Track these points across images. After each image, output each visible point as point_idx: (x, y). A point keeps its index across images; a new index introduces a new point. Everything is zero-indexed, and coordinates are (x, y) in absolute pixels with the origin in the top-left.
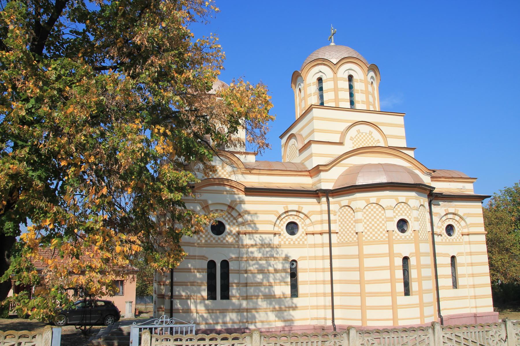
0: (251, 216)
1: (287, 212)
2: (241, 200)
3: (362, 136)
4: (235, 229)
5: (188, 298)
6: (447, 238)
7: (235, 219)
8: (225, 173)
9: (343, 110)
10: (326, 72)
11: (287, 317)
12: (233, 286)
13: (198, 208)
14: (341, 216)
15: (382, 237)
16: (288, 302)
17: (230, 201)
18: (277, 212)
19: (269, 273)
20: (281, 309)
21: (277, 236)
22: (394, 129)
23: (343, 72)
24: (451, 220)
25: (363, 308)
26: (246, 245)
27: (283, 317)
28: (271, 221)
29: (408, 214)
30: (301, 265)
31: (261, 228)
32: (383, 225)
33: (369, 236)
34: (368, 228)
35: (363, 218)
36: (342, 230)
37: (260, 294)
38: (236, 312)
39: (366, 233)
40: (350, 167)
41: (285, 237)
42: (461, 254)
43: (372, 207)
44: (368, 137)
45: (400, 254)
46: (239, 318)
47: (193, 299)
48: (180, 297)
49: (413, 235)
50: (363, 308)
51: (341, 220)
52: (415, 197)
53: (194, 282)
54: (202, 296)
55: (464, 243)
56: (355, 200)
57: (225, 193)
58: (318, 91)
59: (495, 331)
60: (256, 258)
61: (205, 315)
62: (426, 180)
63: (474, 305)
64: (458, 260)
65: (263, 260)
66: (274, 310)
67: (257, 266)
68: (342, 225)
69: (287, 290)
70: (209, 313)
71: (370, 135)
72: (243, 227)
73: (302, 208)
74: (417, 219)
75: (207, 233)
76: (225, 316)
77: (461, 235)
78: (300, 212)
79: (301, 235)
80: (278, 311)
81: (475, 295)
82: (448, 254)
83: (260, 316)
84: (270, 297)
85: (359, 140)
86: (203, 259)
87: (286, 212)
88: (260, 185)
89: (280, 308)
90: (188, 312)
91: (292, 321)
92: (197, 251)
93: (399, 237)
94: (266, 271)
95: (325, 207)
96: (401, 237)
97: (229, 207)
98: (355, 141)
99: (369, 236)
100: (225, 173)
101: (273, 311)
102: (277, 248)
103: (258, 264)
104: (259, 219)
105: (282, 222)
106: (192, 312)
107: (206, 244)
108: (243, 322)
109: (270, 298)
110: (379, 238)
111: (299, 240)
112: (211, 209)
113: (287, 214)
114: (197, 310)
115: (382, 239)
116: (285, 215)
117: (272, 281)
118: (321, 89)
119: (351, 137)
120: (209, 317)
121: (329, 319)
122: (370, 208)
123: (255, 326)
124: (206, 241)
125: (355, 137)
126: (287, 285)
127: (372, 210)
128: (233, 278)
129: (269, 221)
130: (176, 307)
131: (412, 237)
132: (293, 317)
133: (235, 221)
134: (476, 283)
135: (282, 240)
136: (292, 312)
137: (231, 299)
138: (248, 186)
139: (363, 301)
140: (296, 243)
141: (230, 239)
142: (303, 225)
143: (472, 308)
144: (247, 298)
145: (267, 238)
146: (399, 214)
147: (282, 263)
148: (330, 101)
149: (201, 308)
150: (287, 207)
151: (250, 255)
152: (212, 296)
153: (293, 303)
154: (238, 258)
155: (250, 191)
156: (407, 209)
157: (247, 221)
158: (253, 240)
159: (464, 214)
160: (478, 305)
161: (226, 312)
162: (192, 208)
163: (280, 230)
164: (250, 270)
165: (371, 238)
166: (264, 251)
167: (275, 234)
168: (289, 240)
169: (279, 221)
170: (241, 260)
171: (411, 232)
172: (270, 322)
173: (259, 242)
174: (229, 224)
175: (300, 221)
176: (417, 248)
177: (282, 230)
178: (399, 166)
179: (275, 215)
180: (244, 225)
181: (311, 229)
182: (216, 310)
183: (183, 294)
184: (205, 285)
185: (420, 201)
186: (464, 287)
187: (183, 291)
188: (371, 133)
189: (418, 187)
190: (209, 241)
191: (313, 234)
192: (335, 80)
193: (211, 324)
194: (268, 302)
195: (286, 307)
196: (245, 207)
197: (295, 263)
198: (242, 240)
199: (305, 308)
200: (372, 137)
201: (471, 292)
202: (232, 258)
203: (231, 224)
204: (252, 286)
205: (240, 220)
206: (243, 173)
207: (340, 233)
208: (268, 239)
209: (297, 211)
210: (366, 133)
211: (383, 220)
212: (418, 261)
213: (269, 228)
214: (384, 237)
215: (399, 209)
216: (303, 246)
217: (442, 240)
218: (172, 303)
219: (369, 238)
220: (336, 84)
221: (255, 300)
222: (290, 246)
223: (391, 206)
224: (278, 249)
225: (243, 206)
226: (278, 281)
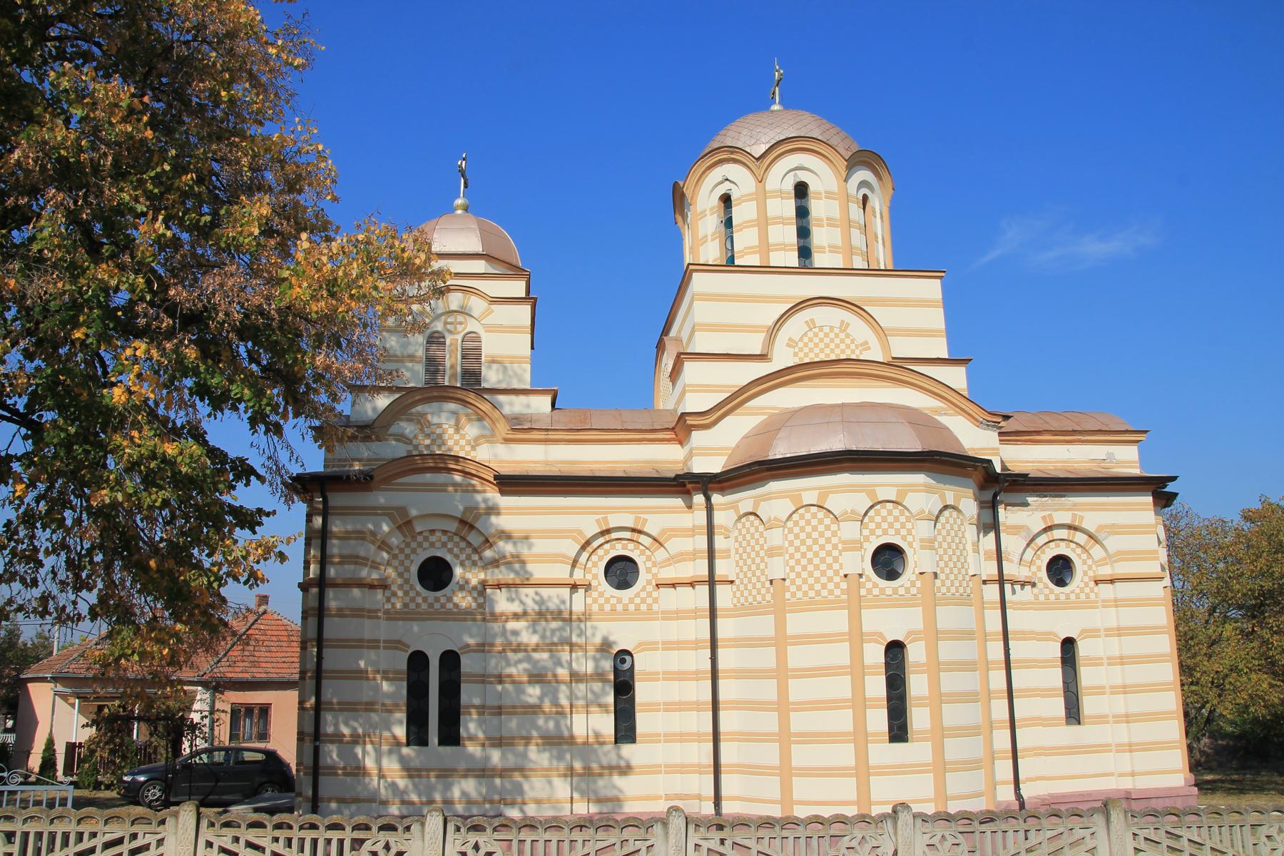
0: (515, 544)
1: (608, 531)
2: (490, 504)
3: (821, 335)
4: (476, 577)
5: (356, 739)
6: (1052, 592)
7: (476, 551)
8: (463, 442)
9: (798, 268)
10: (738, 178)
11: (604, 793)
12: (470, 714)
13: (385, 528)
14: (740, 538)
15: (831, 592)
16: (608, 753)
17: (461, 508)
18: (580, 533)
19: (558, 682)
20: (587, 770)
21: (581, 591)
22: (914, 314)
23: (781, 176)
24: (1063, 544)
25: (786, 772)
26: (502, 614)
27: (595, 792)
28: (564, 556)
29: (904, 532)
30: (642, 663)
31: (539, 571)
32: (836, 560)
33: (799, 588)
34: (798, 568)
35: (787, 544)
36: (741, 576)
37: (535, 733)
38: (477, 776)
39: (793, 582)
40: (772, 415)
41: (601, 594)
42: (1092, 633)
43: (808, 516)
44: (837, 336)
45: (881, 635)
46: (484, 791)
47: (372, 743)
48: (337, 738)
49: (918, 584)
50: (786, 772)
51: (741, 551)
52: (925, 485)
53: (372, 704)
54: (394, 737)
55: (1100, 604)
56: (767, 498)
57: (450, 489)
58: (722, 228)
59: (860, 836)
60: (527, 645)
61: (401, 783)
62: (974, 439)
63: (1129, 769)
64: (1083, 649)
65: (543, 651)
66: (570, 772)
67: (525, 665)
68: (741, 563)
69: (605, 724)
70: (410, 777)
71: (842, 331)
72: (496, 571)
73: (645, 521)
74: (929, 544)
75: (407, 587)
76: (448, 787)
77: (1092, 584)
78: (640, 532)
79: (644, 589)
80: (579, 775)
81: (1139, 738)
82: (1055, 635)
83: (532, 788)
84: (558, 741)
85: (811, 345)
86: (396, 648)
87: (603, 533)
88: (548, 468)
89: (587, 769)
90: (356, 775)
91: (617, 800)
92: (383, 630)
93: (876, 591)
94: (550, 677)
95: (700, 517)
96: (882, 591)
97: (463, 522)
98: (801, 350)
99: (799, 588)
100: (463, 442)
101: (565, 776)
102: (580, 620)
103: (529, 659)
104: (535, 550)
105: (594, 558)
106: (369, 775)
107: (406, 613)
108: (492, 802)
109: (560, 744)
110: (825, 593)
111: (637, 600)
112: (418, 529)
113: (607, 537)
114: (380, 770)
115: (806, 599)
116: (601, 540)
117: (564, 701)
118: (728, 223)
119: (790, 339)
120: (411, 787)
121: (707, 799)
122: (802, 517)
123: (522, 811)
124: (406, 605)
125: (801, 339)
126: (607, 712)
127: (808, 523)
128: (469, 695)
129: (558, 555)
130: (329, 760)
131: (914, 591)
132: (620, 791)
133: (476, 557)
134: (1132, 710)
135: (595, 601)
136: (618, 780)
137: (464, 746)
138: (504, 471)
139: (785, 754)
140: (632, 607)
141: (464, 600)
142: (649, 564)
143: (1121, 775)
144: (499, 742)
145: (555, 597)
146: (879, 532)
147: (595, 659)
148: (749, 250)
149: (391, 766)
150: (605, 519)
151: (513, 639)
152: (417, 735)
153: (620, 757)
154: (483, 645)
155: (512, 484)
156: (902, 519)
157: (504, 557)
158: (517, 603)
159: (1101, 528)
160: (1137, 769)
161: (451, 776)
162: (371, 526)
163: (589, 577)
164: (510, 676)
165: (805, 594)
166: (545, 630)
167: (574, 587)
168: (613, 601)
169: (585, 555)
170: (489, 652)
171: (914, 578)
172: (558, 801)
173: (531, 606)
174: (462, 564)
175: (642, 553)
176: (930, 618)
177: (595, 576)
178: (843, 405)
179: (575, 539)
180: (498, 567)
181: (669, 574)
182: (428, 770)
183: (346, 731)
184: (401, 711)
185: (943, 497)
186: (1101, 719)
187: (347, 724)
188: (844, 326)
189: (943, 462)
190: (412, 606)
191: (674, 585)
192: (762, 197)
193: (412, 803)
194: (555, 753)
195: (602, 767)
196: (501, 522)
197: (628, 658)
198: (492, 602)
199: (653, 769)
200: (848, 336)
201: (1122, 733)
202: (468, 645)
203: (467, 563)
204: (515, 713)
205: (488, 554)
206: (507, 441)
207: (737, 582)
208: (557, 601)
209: (633, 530)
210: (832, 328)
211: (835, 547)
212: (932, 651)
213: (560, 572)
214: (837, 592)
215: (878, 519)
216: (650, 615)
217: (1036, 597)
218: (316, 751)
219: (799, 594)
220: (762, 209)
221: (521, 748)
222: (613, 615)
223: (853, 512)
224: (582, 625)
225: (494, 519)
226: (581, 702)
